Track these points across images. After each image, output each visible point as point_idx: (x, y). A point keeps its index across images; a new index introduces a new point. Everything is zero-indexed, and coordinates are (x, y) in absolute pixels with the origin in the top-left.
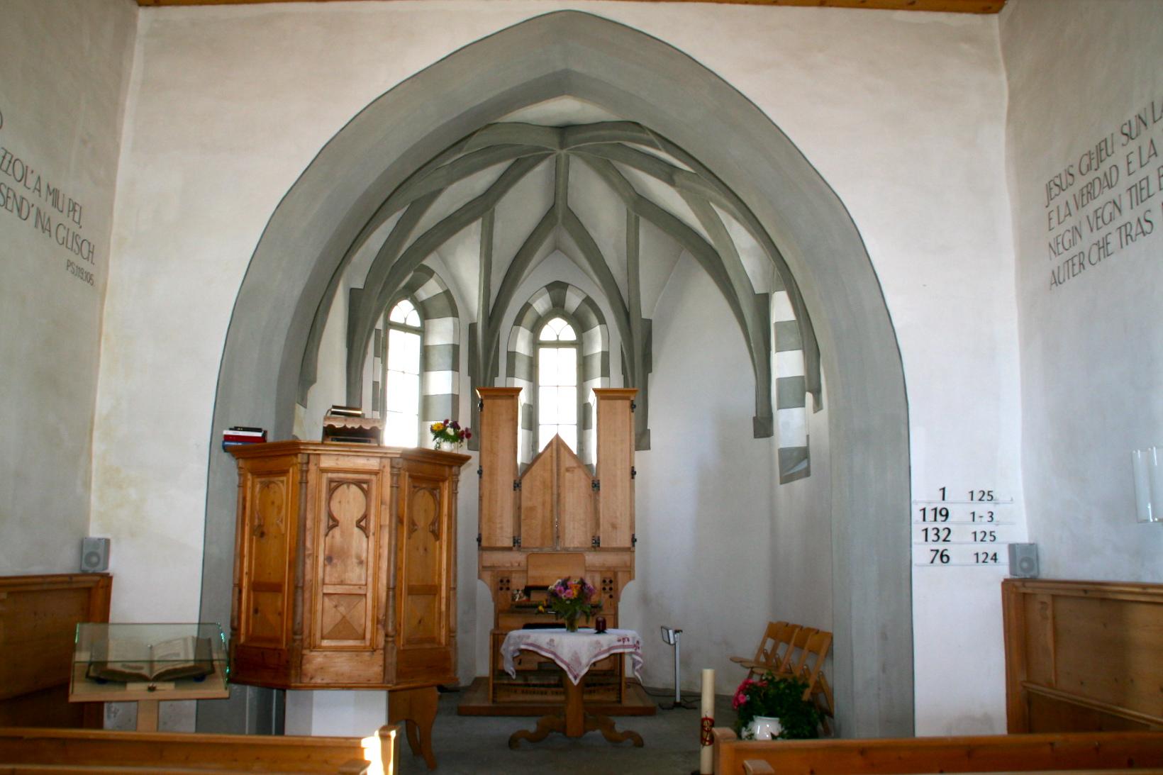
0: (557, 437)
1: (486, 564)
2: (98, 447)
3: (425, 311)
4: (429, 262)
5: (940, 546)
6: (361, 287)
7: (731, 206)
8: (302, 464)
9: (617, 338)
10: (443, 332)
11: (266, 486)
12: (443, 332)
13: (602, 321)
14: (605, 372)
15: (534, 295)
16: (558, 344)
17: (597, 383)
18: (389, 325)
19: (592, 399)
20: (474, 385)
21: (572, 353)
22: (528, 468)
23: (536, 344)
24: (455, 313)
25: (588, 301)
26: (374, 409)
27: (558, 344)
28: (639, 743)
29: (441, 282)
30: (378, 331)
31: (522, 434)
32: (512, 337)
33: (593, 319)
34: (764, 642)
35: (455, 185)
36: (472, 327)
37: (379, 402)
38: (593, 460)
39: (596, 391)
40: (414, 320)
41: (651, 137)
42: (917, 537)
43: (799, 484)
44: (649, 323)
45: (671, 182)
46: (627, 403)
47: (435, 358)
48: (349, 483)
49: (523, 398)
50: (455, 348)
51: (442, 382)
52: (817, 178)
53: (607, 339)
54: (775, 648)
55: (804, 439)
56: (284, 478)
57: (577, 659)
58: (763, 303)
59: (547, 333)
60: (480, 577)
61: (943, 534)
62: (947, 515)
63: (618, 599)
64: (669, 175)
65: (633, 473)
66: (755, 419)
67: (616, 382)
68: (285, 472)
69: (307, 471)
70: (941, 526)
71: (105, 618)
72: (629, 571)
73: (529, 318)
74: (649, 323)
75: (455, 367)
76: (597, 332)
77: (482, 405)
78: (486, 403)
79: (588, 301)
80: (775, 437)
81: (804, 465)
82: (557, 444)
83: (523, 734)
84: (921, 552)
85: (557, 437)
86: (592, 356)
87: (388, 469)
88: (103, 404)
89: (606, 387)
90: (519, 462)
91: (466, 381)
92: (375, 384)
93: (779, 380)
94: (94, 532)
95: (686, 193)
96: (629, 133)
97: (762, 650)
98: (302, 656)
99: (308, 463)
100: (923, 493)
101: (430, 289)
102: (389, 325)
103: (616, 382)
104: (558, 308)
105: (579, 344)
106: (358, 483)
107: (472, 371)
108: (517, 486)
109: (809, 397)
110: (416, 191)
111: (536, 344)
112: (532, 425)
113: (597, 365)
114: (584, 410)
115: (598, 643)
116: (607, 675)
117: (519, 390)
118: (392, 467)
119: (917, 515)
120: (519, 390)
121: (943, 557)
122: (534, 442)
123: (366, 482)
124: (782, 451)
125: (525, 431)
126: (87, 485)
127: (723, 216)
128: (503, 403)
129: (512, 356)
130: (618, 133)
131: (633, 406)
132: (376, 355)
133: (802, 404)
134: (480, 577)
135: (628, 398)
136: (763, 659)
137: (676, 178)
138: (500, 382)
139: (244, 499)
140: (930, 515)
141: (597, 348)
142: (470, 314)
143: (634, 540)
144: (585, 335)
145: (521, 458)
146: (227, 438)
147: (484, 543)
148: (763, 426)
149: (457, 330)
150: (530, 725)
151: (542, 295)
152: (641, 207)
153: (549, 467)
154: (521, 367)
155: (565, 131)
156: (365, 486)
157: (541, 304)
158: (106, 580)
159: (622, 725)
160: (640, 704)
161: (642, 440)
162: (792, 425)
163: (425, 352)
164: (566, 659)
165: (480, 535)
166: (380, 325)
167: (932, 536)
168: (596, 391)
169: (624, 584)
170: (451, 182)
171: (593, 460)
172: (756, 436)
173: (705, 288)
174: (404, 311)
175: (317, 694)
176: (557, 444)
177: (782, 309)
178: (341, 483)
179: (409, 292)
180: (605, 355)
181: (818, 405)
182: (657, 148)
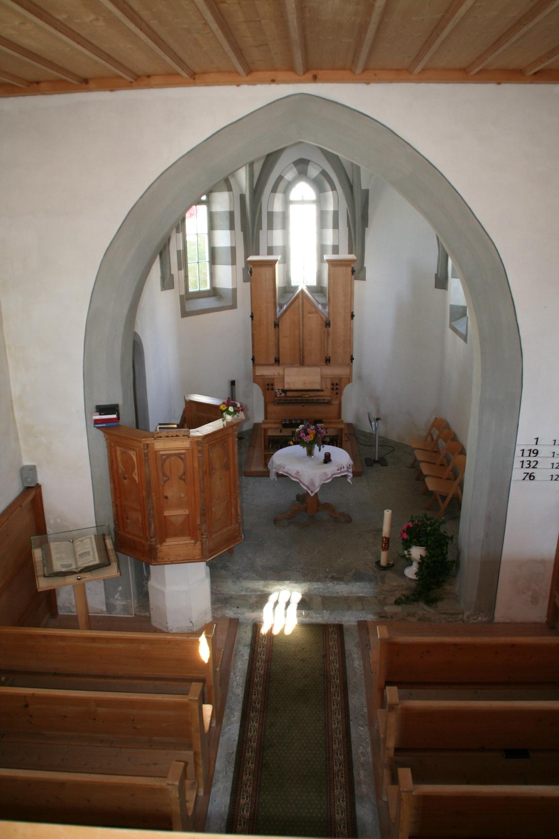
2: (18, 415)
5: (530, 471)
10: (222, 202)
12: (222, 202)
13: (334, 188)
16: (303, 202)
23: (287, 202)
24: (230, 189)
25: (324, 173)
26: (180, 269)
27: (303, 202)
32: (271, 201)
36: (242, 197)
42: (517, 464)
44: (367, 192)
46: (350, 269)
47: (218, 221)
50: (231, 214)
51: (223, 239)
52: (481, 229)
53: (337, 202)
57: (313, 483)
61: (533, 464)
62: (537, 453)
63: (341, 395)
65: (352, 316)
66: (436, 275)
70: (532, 459)
71: (46, 533)
74: (367, 192)
75: (232, 227)
77: (251, 272)
79: (324, 173)
84: (518, 473)
88: (16, 390)
91: (240, 235)
92: (179, 252)
94: (26, 462)
98: (156, 549)
100: (524, 440)
104: (303, 174)
107: (244, 228)
108: (276, 325)
115: (325, 474)
119: (518, 453)
121: (531, 477)
126: (17, 439)
128: (266, 271)
129: (271, 215)
140: (526, 453)
141: (330, 208)
142: (241, 189)
146: (96, 422)
148: (441, 282)
149: (232, 201)
158: (38, 487)
164: (306, 484)
167: (526, 465)
169: (345, 385)
172: (436, 287)
175: (168, 568)
180: (336, 214)
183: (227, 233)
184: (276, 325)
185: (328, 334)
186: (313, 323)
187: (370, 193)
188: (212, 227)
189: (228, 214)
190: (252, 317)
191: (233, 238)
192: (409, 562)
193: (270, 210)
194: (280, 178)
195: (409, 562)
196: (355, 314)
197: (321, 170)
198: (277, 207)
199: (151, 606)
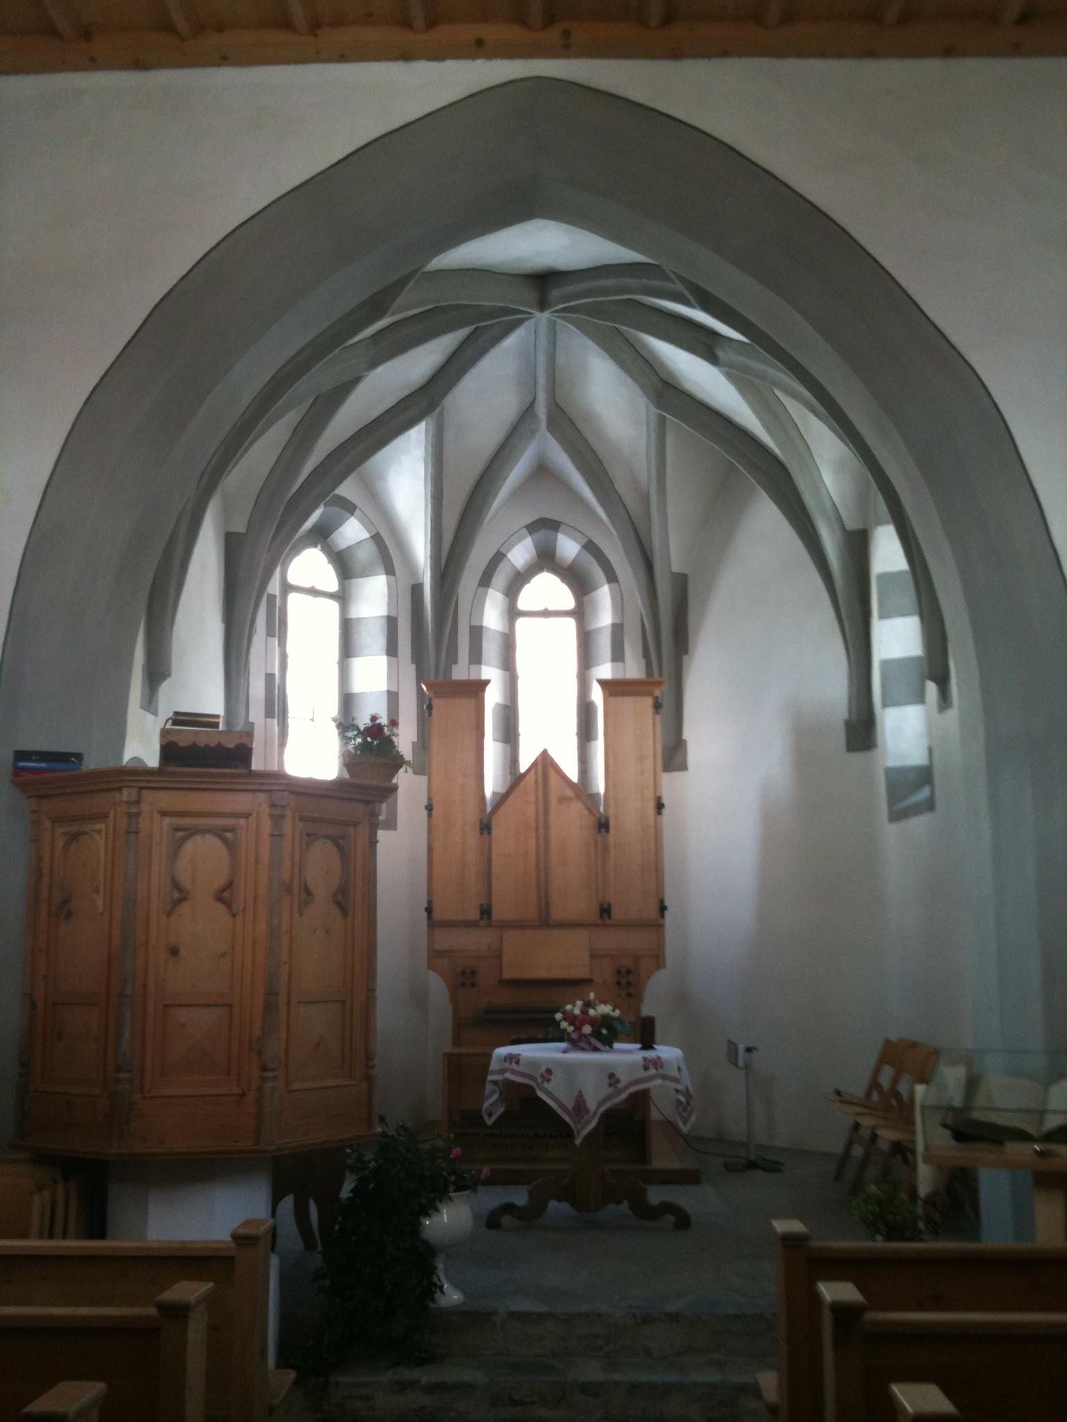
0: (545, 754)
1: (437, 947)
3: (344, 564)
4: (346, 489)
6: (242, 530)
7: (806, 393)
8: (129, 803)
9: (637, 603)
11: (74, 837)
12: (374, 597)
13: (612, 578)
14: (618, 656)
15: (510, 542)
17: (605, 670)
18: (287, 588)
19: (597, 695)
20: (420, 677)
21: (570, 624)
22: (501, 799)
23: (513, 613)
26: (269, 713)
28: (683, 1221)
29: (367, 523)
30: (272, 598)
31: (492, 750)
33: (598, 573)
34: (877, 1072)
35: (380, 370)
37: (276, 706)
38: (600, 786)
39: (603, 683)
40: (328, 579)
41: (679, 287)
43: (918, 823)
45: (712, 359)
46: (649, 701)
48: (203, 831)
49: (493, 697)
50: (391, 623)
51: (373, 675)
53: (620, 605)
54: (895, 1081)
55: (925, 753)
56: (102, 826)
58: (858, 546)
59: (529, 597)
60: (430, 967)
64: (704, 344)
67: (633, 669)
68: (103, 817)
69: (138, 814)
72: (658, 960)
73: (501, 578)
76: (604, 595)
77: (430, 707)
78: (435, 702)
80: (877, 753)
81: (925, 793)
82: (545, 762)
83: (509, 1208)
85: (545, 754)
86: (599, 630)
87: (265, 810)
89: (619, 676)
90: (488, 791)
91: (409, 671)
92: (269, 678)
93: (886, 664)
95: (741, 379)
96: (645, 281)
97: (874, 1084)
99: (138, 802)
101: (352, 532)
102: (287, 588)
103: (633, 669)
104: (546, 559)
105: (581, 614)
106: (219, 833)
107: (418, 656)
108: (485, 827)
109: (931, 688)
110: (320, 378)
111: (513, 613)
112: (509, 734)
113: (604, 644)
114: (585, 711)
116: (628, 1121)
117: (487, 682)
118: (272, 805)
120: (487, 682)
122: (512, 759)
123: (232, 830)
124: (891, 773)
125: (499, 746)
127: (795, 409)
128: (464, 704)
129: (477, 632)
130: (628, 281)
131: (657, 706)
132: (270, 633)
133: (920, 698)
134: (430, 967)
135: (650, 694)
136: (875, 1097)
137: (720, 354)
138: (460, 672)
139: (40, 859)
141: (605, 617)
143: (663, 909)
144: (585, 599)
145: (492, 783)
147: (437, 915)
148: (862, 731)
150: (520, 1197)
151: (520, 540)
152: (667, 393)
153: (532, 799)
154: (491, 649)
155: (544, 283)
156: (229, 835)
157: (521, 554)
159: (656, 1195)
160: (676, 1165)
161: (674, 754)
162: (905, 731)
163: (347, 629)
165: (430, 903)
166: (274, 587)
168: (603, 683)
170: (374, 364)
171: (600, 786)
172: (395, 829)
173: (765, 519)
174: (309, 567)
176: (545, 762)
177: (887, 554)
178: (191, 832)
179: (322, 535)
180: (618, 629)
181: (945, 699)
182: (692, 306)
183: (382, 661)
184: (485, 827)
185: (606, 848)
186: (570, 825)
187: (690, 580)
188: (348, 649)
189: (384, 622)
190: (429, 808)
191: (393, 673)
192: (449, 1174)
193: (474, 623)
194: (499, 557)
195: (449, 1174)
196: (665, 801)
197: (584, 541)
198: (492, 617)
199: (620, 699)
